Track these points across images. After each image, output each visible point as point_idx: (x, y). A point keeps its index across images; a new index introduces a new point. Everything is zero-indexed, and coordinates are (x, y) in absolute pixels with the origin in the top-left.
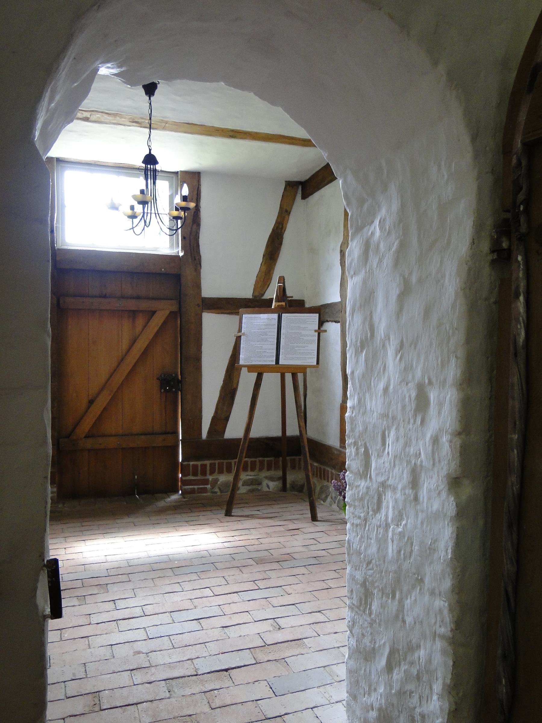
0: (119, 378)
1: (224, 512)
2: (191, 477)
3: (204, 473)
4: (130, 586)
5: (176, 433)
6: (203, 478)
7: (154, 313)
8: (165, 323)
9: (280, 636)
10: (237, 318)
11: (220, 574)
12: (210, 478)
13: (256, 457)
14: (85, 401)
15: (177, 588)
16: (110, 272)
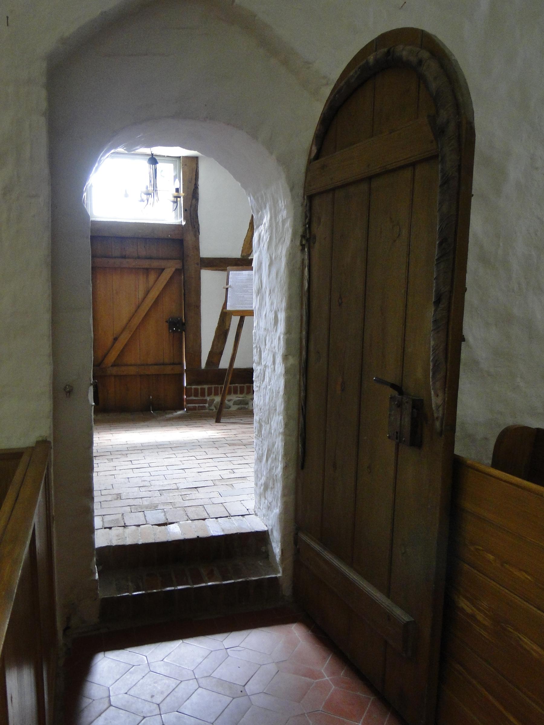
0: (137, 320)
1: (215, 420)
2: (193, 398)
3: (203, 394)
4: (143, 455)
5: (181, 364)
7: (163, 270)
8: (171, 278)
9: (233, 476)
10: (224, 273)
11: (203, 450)
12: (208, 399)
13: (244, 383)
14: (111, 339)
15: (174, 456)
16: (127, 238)
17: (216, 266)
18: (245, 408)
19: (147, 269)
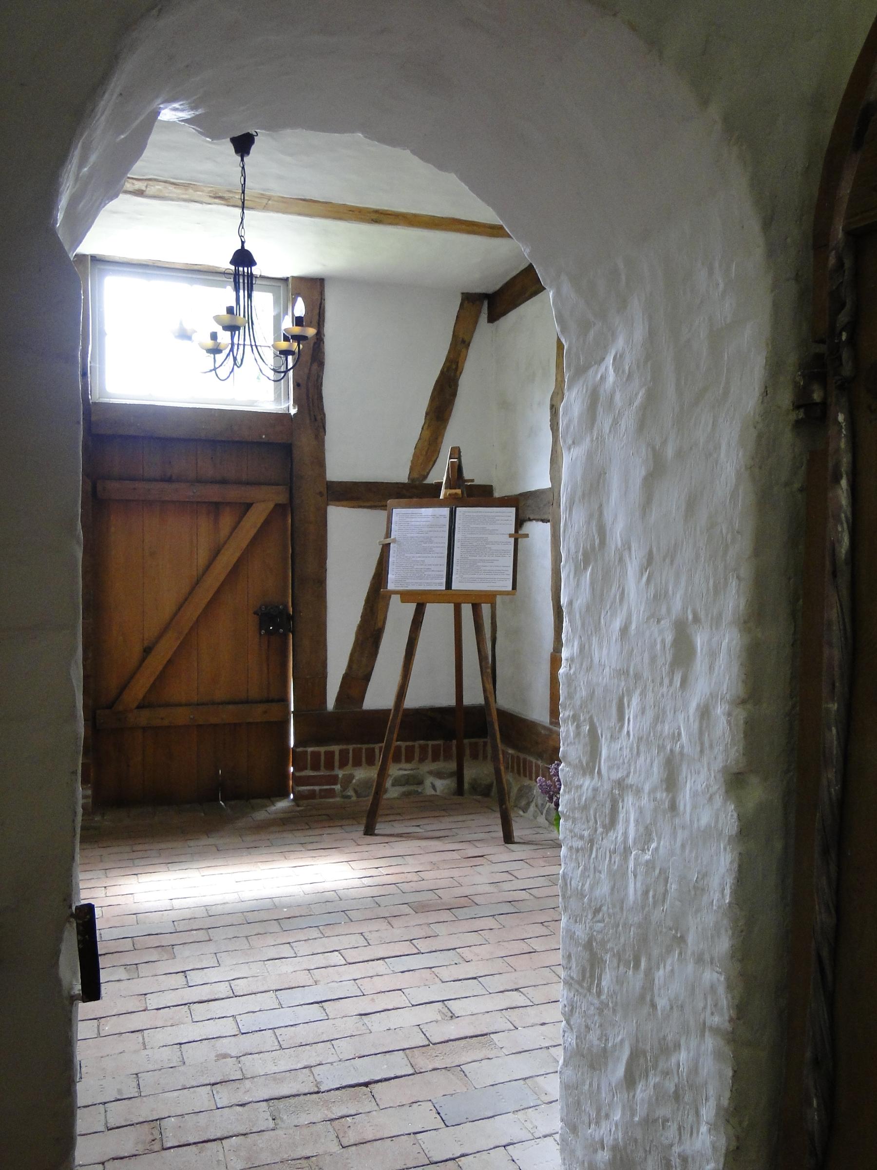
0: (192, 612)
1: (362, 828)
2: (309, 773)
3: (330, 765)
4: (211, 948)
5: (285, 700)
6: (328, 773)
7: (248, 506)
8: (266, 523)
9: (452, 1030)
10: (383, 514)
11: (356, 928)
12: (340, 773)
13: (415, 740)
14: (137, 650)
15: (286, 951)
16: (178, 440)
17: (357, 499)
18: (417, 793)
19: (217, 505)
